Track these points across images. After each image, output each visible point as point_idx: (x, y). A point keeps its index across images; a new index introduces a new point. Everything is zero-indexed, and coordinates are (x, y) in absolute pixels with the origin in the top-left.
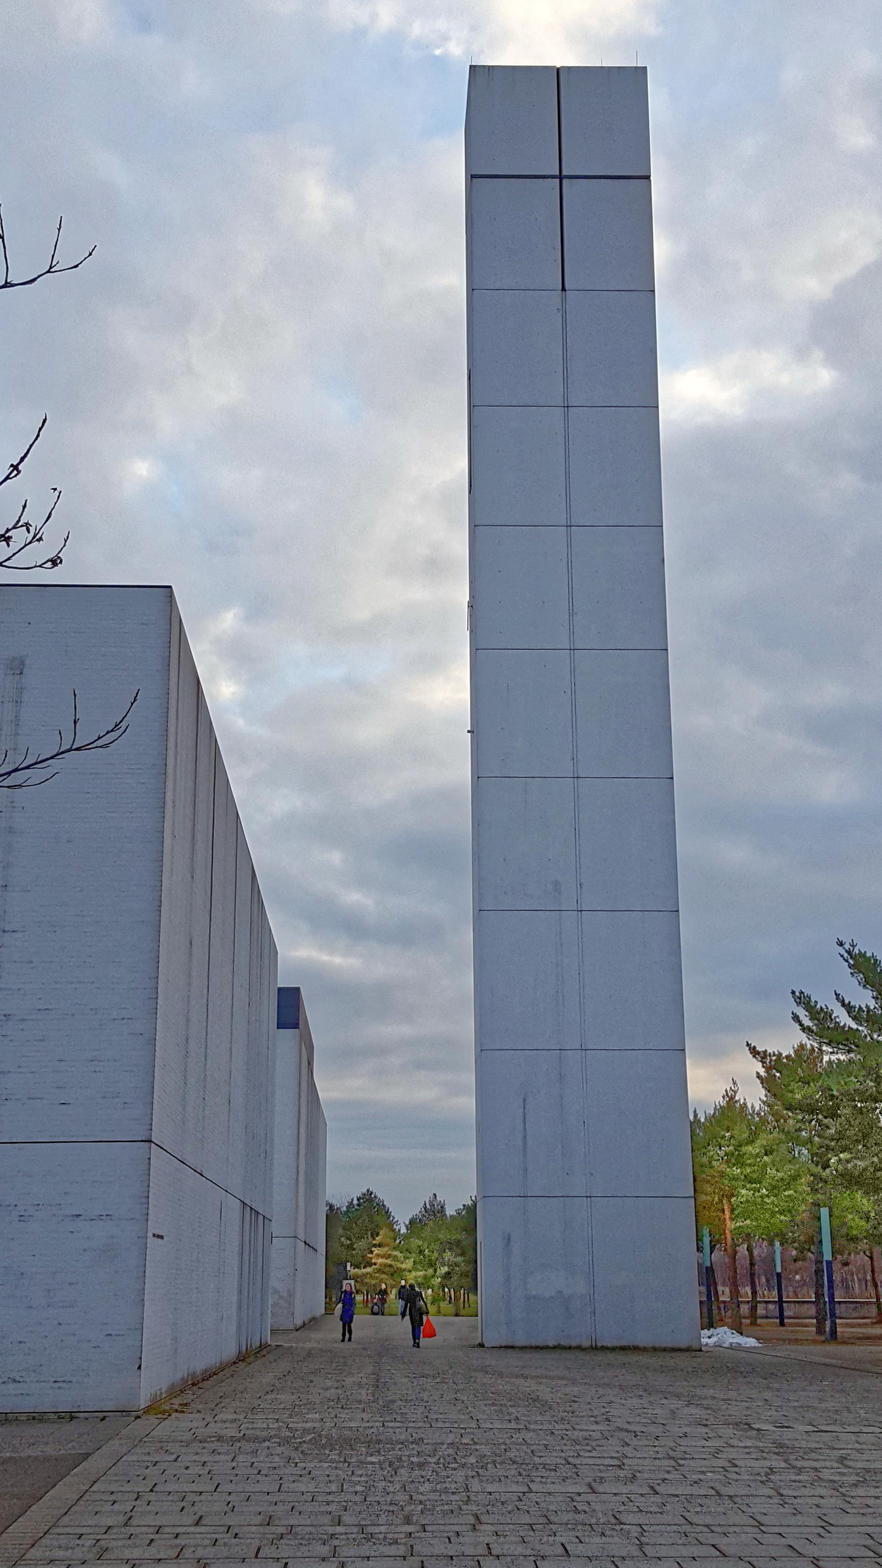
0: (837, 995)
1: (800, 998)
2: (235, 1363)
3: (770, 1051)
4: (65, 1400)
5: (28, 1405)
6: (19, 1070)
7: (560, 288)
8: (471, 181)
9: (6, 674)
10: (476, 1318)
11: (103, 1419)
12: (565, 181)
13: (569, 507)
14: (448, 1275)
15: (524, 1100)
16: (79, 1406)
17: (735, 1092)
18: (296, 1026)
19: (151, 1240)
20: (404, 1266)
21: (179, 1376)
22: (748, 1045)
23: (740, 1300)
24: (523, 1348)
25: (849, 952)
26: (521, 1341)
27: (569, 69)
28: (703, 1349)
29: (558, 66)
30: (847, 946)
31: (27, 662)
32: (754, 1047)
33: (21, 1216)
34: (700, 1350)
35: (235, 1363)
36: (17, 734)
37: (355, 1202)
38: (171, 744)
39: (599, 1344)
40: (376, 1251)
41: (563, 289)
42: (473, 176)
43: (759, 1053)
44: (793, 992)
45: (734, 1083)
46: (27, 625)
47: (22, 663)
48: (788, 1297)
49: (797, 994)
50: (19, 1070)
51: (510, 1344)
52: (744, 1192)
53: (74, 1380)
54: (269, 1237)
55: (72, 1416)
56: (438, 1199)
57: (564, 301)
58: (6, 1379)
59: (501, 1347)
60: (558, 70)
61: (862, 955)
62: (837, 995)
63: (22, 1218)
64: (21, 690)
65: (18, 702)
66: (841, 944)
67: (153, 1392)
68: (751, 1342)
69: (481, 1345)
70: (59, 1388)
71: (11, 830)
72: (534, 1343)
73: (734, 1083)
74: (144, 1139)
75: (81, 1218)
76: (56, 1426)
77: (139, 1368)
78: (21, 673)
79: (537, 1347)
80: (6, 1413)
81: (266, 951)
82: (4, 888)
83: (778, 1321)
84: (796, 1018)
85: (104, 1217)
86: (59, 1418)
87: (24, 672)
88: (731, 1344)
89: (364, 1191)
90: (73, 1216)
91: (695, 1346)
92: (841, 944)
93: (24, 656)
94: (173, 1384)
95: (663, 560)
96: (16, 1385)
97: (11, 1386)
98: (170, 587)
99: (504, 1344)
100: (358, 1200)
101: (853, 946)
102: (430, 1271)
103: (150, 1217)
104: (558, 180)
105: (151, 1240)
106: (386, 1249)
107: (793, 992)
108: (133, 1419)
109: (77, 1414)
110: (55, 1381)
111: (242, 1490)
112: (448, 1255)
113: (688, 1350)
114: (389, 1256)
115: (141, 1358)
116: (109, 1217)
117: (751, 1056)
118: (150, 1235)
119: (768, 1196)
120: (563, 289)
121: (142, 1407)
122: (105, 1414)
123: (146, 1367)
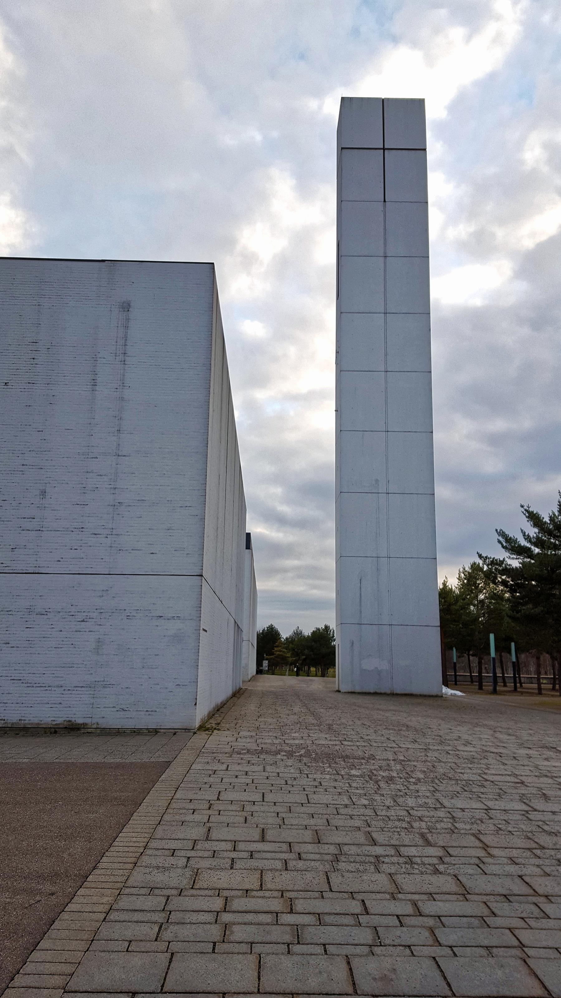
0: (522, 530)
1: (500, 532)
2: (232, 698)
3: (489, 556)
4: (150, 722)
5: (130, 724)
6: (127, 534)
7: (383, 201)
8: (341, 152)
9: (120, 311)
10: (334, 678)
11: (175, 734)
12: (386, 151)
13: (386, 304)
14: (304, 660)
15: (360, 580)
16: (161, 726)
17: (447, 582)
18: (249, 549)
19: (201, 631)
20: (287, 655)
21: (212, 707)
22: (477, 553)
23: (473, 674)
24: (359, 693)
25: (526, 510)
26: (358, 689)
27: (388, 99)
28: (443, 696)
29: (383, 98)
30: (525, 507)
31: (132, 304)
32: (481, 555)
33: (128, 616)
34: (442, 697)
35: (232, 698)
36: (125, 345)
37: (266, 629)
38: (213, 353)
39: (395, 692)
40: (276, 649)
41: (385, 201)
42: (342, 148)
43: (483, 557)
44: (496, 530)
45: (446, 578)
46: (131, 283)
47: (129, 305)
48: (546, 674)
49: (499, 531)
50: (127, 534)
51: (353, 691)
52: (451, 626)
53: (158, 710)
54: (242, 640)
55: (156, 731)
56: (300, 628)
57: (385, 206)
58: (119, 709)
59: (349, 692)
60: (383, 100)
61: (532, 512)
62: (522, 530)
63: (128, 617)
64: (128, 320)
65: (127, 327)
66: (522, 506)
67: (202, 718)
68: (459, 693)
69: (339, 691)
70: (149, 715)
71: (122, 399)
72: (364, 691)
73: (446, 578)
74: (198, 574)
75: (163, 618)
76: (148, 738)
77: (196, 704)
78: (128, 311)
79: (393, 695)
80: (118, 729)
81: (243, 506)
82: (118, 432)
83: (454, 683)
84: (499, 542)
85: (175, 618)
86: (149, 732)
87: (129, 310)
88: (451, 694)
89: (270, 624)
90: (158, 617)
91: (439, 694)
92: (522, 506)
93: (130, 301)
94: (210, 712)
95: (430, 330)
96: (124, 712)
97: (122, 713)
98: (213, 264)
99: (350, 691)
100: (267, 628)
101: (529, 507)
102: (297, 658)
103: (202, 619)
104: (382, 150)
105: (201, 631)
106: (280, 648)
107: (496, 530)
108: (192, 734)
109: (160, 730)
110: (147, 711)
111: (282, 801)
112: (306, 652)
113: (436, 696)
114: (280, 651)
115: (196, 699)
116: (178, 618)
117: (479, 559)
118: (201, 629)
119: (462, 628)
120: (385, 201)
121: (197, 727)
122: (176, 730)
123: (199, 704)
